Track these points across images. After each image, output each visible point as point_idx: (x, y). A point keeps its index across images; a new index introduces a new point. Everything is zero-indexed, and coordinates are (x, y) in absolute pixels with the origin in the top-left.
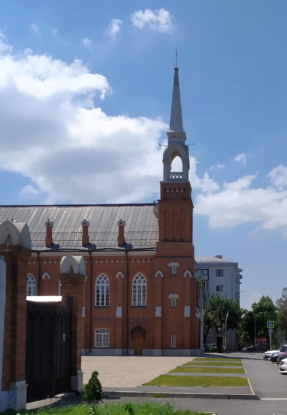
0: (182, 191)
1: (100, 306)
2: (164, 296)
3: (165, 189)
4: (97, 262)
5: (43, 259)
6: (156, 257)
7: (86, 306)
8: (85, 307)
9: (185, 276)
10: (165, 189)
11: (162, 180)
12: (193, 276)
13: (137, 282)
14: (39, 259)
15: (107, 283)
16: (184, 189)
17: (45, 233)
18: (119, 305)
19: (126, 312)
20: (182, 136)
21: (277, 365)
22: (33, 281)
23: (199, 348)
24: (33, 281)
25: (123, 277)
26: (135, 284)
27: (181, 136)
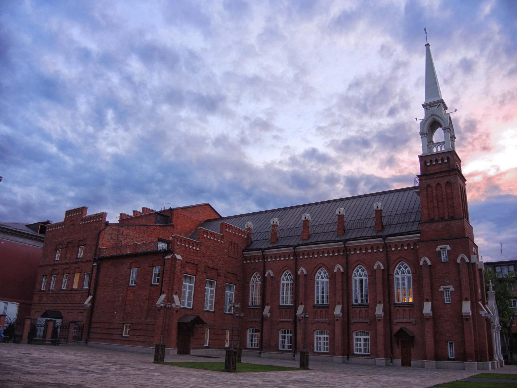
0: (446, 161)
1: (401, 302)
2: (433, 289)
3: (425, 162)
4: (353, 253)
5: (350, 249)
6: (419, 241)
7: (343, 304)
8: (382, 305)
9: (458, 261)
10: (425, 162)
11: (421, 153)
12: (470, 259)
13: (285, 280)
14: (296, 254)
15: (409, 273)
16: (448, 158)
17: (336, 223)
18: (177, 311)
19: (387, 311)
20: (440, 105)
21: (310, 375)
22: (325, 275)
23: (492, 358)
24: (325, 275)
25: (382, 268)
26: (283, 282)
27: (438, 104)
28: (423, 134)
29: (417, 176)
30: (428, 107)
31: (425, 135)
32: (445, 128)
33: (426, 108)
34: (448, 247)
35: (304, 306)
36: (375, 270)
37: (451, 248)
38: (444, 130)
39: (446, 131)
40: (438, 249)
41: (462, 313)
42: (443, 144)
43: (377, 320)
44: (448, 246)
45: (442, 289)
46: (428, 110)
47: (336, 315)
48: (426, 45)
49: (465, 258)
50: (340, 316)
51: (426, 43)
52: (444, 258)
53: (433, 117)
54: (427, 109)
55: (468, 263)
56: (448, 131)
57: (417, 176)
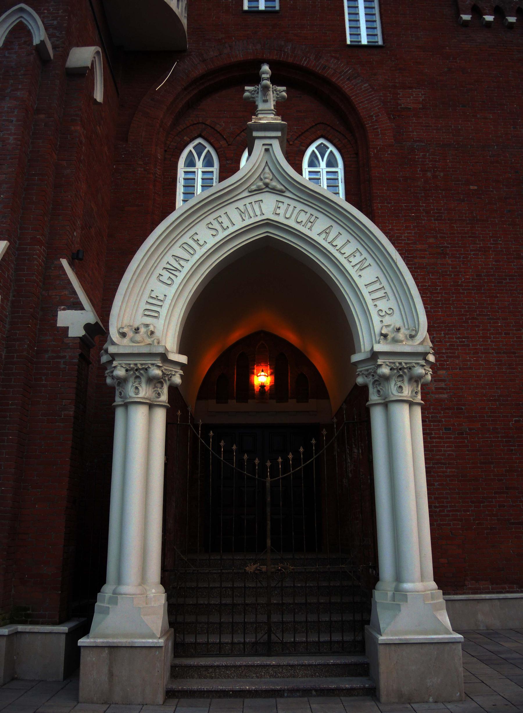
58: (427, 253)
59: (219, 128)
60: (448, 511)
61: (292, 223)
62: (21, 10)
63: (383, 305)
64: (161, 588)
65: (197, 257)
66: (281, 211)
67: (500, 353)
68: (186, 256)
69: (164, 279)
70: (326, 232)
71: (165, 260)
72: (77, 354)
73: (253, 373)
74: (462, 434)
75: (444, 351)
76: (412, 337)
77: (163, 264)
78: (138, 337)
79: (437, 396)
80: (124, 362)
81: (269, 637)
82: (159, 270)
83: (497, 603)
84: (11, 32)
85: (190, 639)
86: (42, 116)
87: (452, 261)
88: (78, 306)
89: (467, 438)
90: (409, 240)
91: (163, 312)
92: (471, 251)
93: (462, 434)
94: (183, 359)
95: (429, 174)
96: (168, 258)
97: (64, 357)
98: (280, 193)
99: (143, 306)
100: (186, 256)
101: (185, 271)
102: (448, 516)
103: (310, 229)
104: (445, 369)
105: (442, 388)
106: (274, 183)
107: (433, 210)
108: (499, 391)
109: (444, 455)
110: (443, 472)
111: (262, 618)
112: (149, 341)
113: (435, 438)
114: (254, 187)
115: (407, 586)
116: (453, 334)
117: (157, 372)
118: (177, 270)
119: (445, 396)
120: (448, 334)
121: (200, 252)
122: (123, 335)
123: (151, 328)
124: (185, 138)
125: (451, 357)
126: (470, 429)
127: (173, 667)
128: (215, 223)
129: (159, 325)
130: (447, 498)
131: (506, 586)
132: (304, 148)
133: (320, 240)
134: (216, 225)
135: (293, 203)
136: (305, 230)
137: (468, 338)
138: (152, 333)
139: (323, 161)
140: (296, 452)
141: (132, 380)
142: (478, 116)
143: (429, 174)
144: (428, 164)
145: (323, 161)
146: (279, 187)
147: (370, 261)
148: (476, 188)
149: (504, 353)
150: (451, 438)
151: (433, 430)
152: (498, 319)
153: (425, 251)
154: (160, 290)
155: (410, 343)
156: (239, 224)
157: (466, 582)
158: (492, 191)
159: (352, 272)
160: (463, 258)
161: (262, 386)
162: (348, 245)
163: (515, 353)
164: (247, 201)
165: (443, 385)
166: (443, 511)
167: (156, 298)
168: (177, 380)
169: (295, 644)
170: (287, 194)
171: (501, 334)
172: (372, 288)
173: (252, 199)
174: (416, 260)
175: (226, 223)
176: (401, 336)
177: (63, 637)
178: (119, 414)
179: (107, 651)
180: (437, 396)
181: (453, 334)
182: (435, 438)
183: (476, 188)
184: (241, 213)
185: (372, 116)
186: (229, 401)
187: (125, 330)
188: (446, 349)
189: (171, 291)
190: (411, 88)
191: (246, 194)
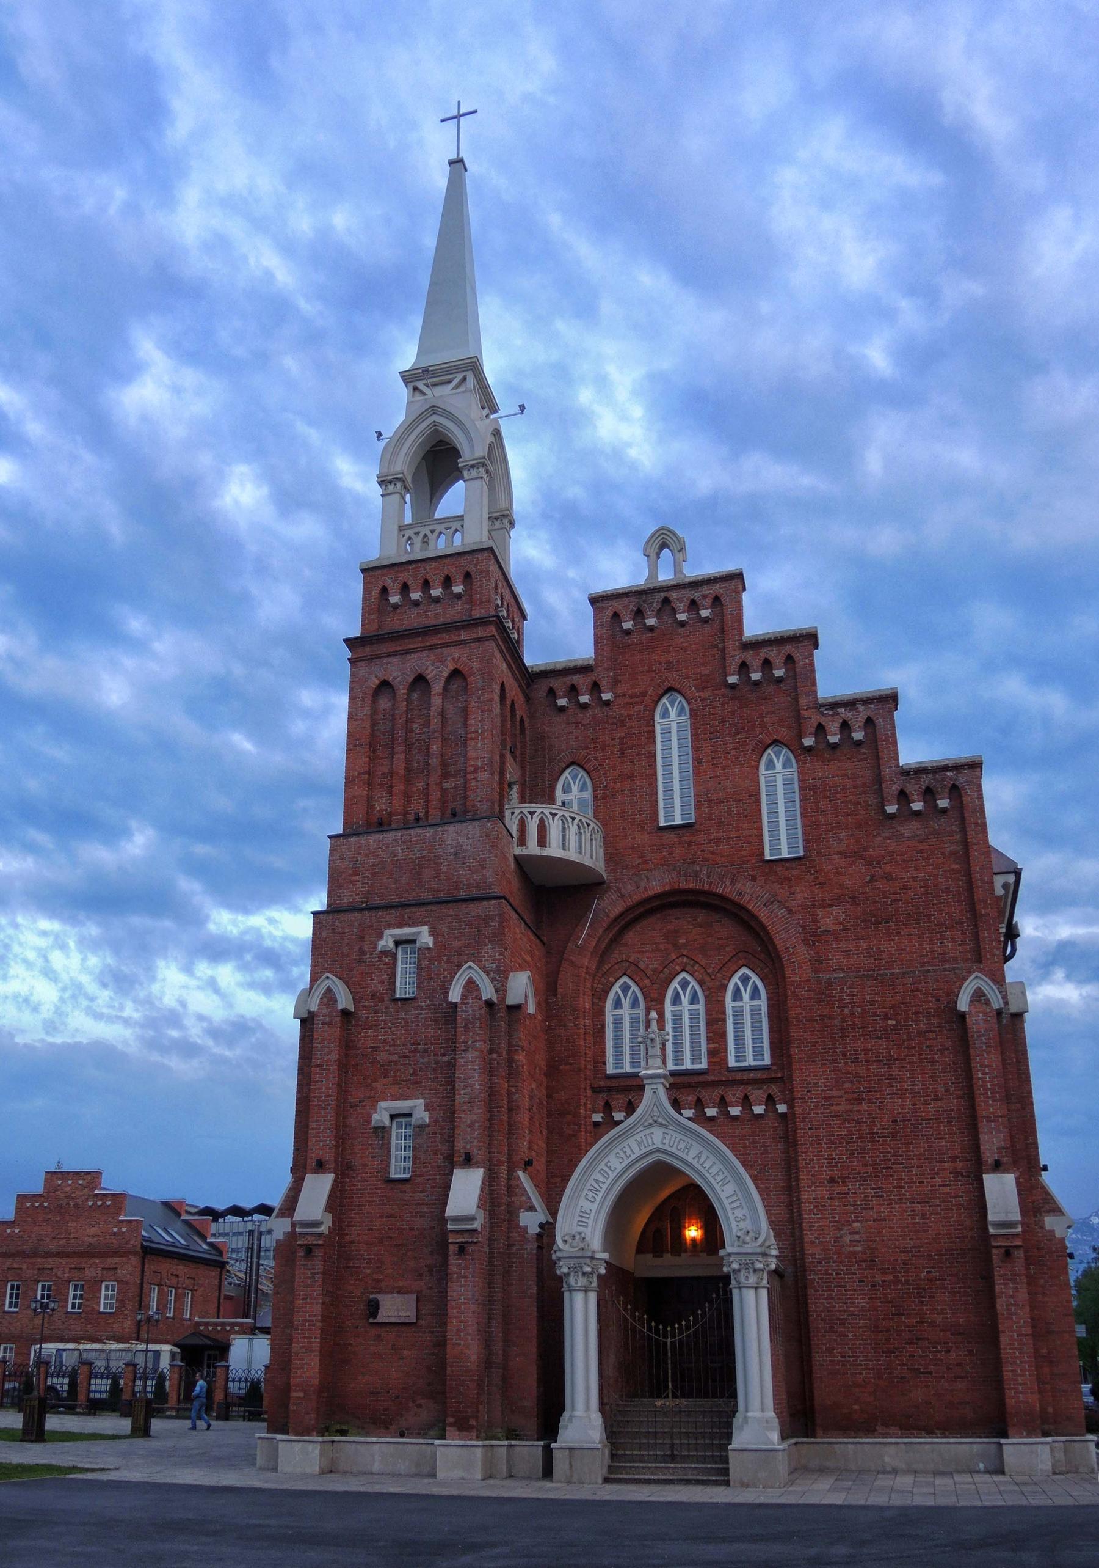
20: (464, 379)
27: (459, 377)
28: (390, 482)
29: (346, 641)
30: (420, 385)
31: (399, 485)
32: (471, 463)
33: (415, 389)
34: (425, 937)
35: (332, 1176)
36: (455, 1005)
37: (435, 943)
38: (384, 487)
39: (391, 488)
40: (386, 942)
41: (444, 1220)
42: (456, 525)
43: (452, 1249)
44: (425, 929)
45: (381, 1116)
46: (419, 397)
47: (456, 1219)
48: (451, 163)
49: (478, 982)
50: (324, 1229)
51: (454, 156)
52: (405, 984)
53: (435, 418)
54: (417, 393)
55: (489, 1004)
56: (480, 475)
57: (346, 641)
58: (844, 1099)
59: (642, 965)
60: (861, 1361)
61: (674, 1150)
62: (470, 967)
63: (739, 1213)
64: (600, 1414)
65: (610, 1180)
66: (666, 1141)
67: (914, 1203)
68: (603, 1179)
69: (589, 1197)
70: (698, 1156)
71: (588, 1185)
72: (535, 1246)
73: (685, 1228)
74: (875, 1286)
75: (859, 1203)
76: (756, 1239)
77: (588, 1186)
78: (575, 1243)
79: (851, 1249)
80: (567, 1262)
81: (672, 1451)
82: (585, 1191)
83: (903, 1446)
84: (464, 987)
85: (620, 1452)
86: (495, 1056)
87: (869, 1107)
88: (532, 1209)
89: (879, 1290)
90: (825, 1086)
91: (590, 1222)
92: (888, 1094)
93: (875, 1286)
94: (606, 1256)
95: (847, 1011)
96: (591, 1181)
97: (527, 1249)
98: (666, 1126)
99: (577, 1218)
100: (603, 1179)
101: (603, 1191)
102: (861, 1365)
103: (687, 1154)
104: (859, 1221)
105: (857, 1241)
106: (660, 1120)
107: (850, 1051)
108: (911, 1242)
109: (858, 1307)
110: (857, 1323)
111: (668, 1441)
112: (581, 1245)
113: (849, 1290)
114: (646, 1124)
115: (750, 1414)
116: (868, 1185)
117: (589, 1269)
118: (597, 1190)
119: (859, 1249)
120: (862, 1185)
121: (612, 1176)
122: (565, 1242)
123: (583, 1235)
124: (611, 979)
125: (865, 1209)
126: (884, 1281)
127: (609, 1467)
128: (621, 1152)
129: (587, 1232)
130: (860, 1348)
131: (915, 1432)
132: (726, 982)
133: (694, 1163)
134: (622, 1155)
135: (675, 1134)
136: (684, 1156)
137: (882, 1188)
138: (584, 1238)
139: (746, 990)
140: (688, 1321)
141: (572, 1274)
142: (902, 933)
143: (847, 1011)
144: (845, 999)
145: (746, 990)
146: (664, 1122)
147: (729, 1178)
148: (894, 1022)
149: (918, 1203)
150: (864, 1290)
151: (847, 1282)
152: (913, 1167)
153: (841, 1097)
154: (587, 1206)
155: (754, 1244)
156: (638, 1153)
157: (877, 1428)
158: (911, 1025)
159: (717, 1187)
160: (880, 1102)
161: (694, 1240)
162: (714, 1167)
163: (928, 1202)
164: (642, 1134)
165: (857, 1237)
166: (856, 1361)
167: (585, 1212)
168: (603, 1271)
169: (689, 1456)
170: (670, 1127)
171: (915, 1183)
172: (731, 1200)
173: (649, 1131)
174: (832, 1108)
175: (629, 1153)
176: (748, 1239)
177: (541, 1448)
178: (566, 1295)
179: (568, 1451)
180: (851, 1249)
181: (868, 1185)
182: (849, 1290)
183: (894, 1022)
184: (639, 1144)
185: (788, 948)
186: (664, 1255)
187: (566, 1238)
188: (861, 1201)
189: (594, 1207)
190: (831, 906)
191: (641, 1129)
